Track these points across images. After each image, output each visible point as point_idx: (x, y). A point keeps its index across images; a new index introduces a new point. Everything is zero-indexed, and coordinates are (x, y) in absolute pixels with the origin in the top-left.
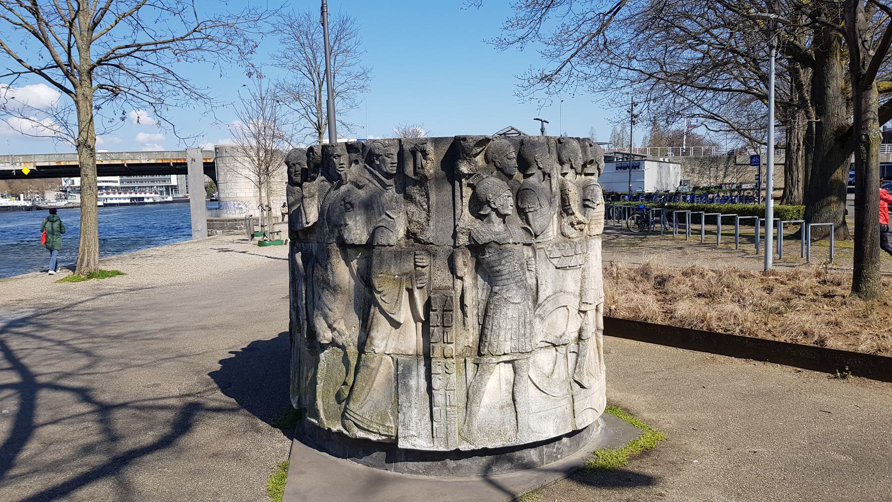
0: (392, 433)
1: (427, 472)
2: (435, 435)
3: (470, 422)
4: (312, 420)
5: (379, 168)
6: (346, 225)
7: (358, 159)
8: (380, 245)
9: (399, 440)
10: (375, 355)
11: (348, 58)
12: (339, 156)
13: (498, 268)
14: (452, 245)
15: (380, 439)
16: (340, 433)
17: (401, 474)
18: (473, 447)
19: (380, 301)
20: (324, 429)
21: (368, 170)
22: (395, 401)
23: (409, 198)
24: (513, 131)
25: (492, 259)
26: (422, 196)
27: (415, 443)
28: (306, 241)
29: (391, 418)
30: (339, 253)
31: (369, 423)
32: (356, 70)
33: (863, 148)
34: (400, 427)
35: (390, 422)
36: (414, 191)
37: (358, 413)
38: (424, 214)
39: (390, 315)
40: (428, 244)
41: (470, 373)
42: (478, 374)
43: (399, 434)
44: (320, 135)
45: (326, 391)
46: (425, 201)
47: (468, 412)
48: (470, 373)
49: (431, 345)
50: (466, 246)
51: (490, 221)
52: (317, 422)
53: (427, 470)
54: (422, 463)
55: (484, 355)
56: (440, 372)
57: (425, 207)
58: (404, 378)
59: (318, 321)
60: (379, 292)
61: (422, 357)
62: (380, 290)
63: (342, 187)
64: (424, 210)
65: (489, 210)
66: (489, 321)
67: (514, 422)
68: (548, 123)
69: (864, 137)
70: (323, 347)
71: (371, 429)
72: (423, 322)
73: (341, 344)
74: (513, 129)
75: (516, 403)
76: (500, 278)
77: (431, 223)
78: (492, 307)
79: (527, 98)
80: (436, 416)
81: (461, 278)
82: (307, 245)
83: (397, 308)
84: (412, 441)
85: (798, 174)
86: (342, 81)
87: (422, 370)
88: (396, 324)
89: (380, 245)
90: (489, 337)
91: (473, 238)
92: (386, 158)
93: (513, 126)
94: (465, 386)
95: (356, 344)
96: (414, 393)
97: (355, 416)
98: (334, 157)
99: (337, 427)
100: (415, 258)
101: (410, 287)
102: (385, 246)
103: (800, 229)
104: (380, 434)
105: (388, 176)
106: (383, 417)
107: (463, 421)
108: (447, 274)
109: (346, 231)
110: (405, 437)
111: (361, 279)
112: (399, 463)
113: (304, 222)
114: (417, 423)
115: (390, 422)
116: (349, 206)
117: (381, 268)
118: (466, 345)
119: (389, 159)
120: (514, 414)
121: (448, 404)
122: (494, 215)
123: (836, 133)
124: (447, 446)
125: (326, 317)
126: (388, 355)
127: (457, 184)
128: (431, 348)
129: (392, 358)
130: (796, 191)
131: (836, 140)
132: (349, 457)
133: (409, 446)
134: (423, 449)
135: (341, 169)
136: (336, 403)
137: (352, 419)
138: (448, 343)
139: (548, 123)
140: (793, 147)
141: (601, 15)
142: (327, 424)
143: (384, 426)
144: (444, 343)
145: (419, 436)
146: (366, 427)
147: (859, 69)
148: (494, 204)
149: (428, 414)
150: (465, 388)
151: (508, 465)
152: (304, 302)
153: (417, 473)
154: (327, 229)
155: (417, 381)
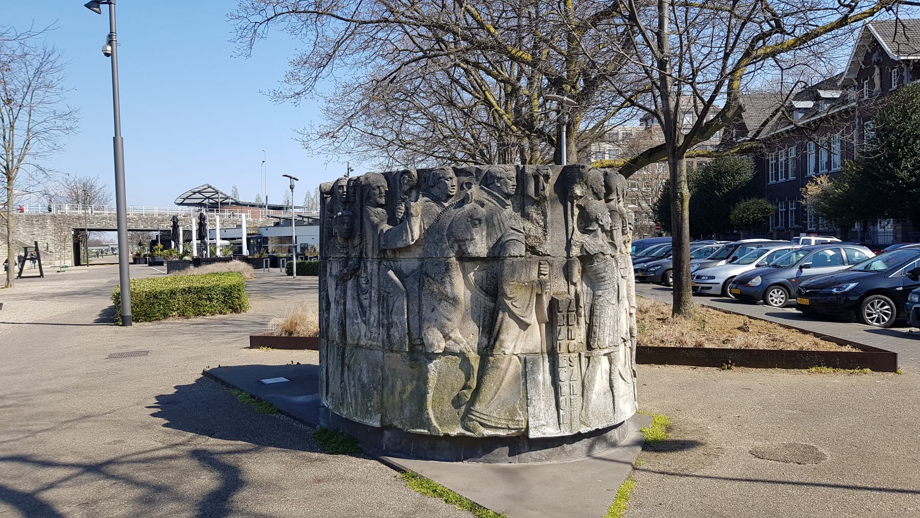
0: (522, 425)
1: (548, 458)
2: (561, 422)
3: (587, 407)
4: (417, 430)
5: (499, 190)
6: (472, 239)
7: (471, 182)
8: (511, 256)
9: (530, 431)
10: (505, 356)
11: (47, 94)
12: (451, 178)
13: (603, 275)
14: (565, 256)
15: (509, 433)
16: (461, 437)
17: (526, 464)
18: (589, 429)
19: (511, 306)
20: (440, 436)
21: (486, 191)
22: (523, 396)
23: (526, 216)
24: (210, 190)
25: (600, 267)
26: (538, 214)
27: (545, 431)
28: (394, 260)
29: (521, 413)
30: (458, 266)
31: (496, 421)
32: (61, 108)
33: (678, 202)
34: (530, 419)
35: (520, 416)
36: (532, 211)
37: (485, 413)
38: (540, 230)
39: (522, 318)
40: (545, 255)
41: (584, 365)
42: (590, 365)
43: (530, 425)
44: (8, 180)
45: (438, 401)
46: (541, 219)
47: (585, 399)
48: (584, 365)
49: (558, 342)
50: (577, 257)
51: (596, 236)
52: (426, 431)
53: (550, 456)
54: (544, 450)
55: (593, 349)
56: (566, 365)
57: (542, 224)
58: (533, 374)
59: (430, 332)
60: (511, 299)
61: (546, 355)
62: (511, 296)
63: (466, 206)
64: (540, 226)
65: (596, 227)
66: (596, 320)
67: (612, 405)
68: (297, 180)
69: (679, 194)
70: (431, 357)
71: (500, 426)
72: (547, 324)
73: (459, 352)
74: (209, 187)
75: (613, 388)
76: (603, 283)
77: (548, 238)
78: (598, 308)
79: (315, 152)
80: (562, 404)
81: (575, 284)
82: (395, 263)
83: (529, 312)
84: (543, 430)
86: (40, 120)
87: (547, 365)
88: (524, 326)
89: (511, 256)
90: (597, 333)
91: (585, 250)
92: (509, 181)
93: (210, 184)
94: (580, 376)
95: (476, 349)
96: (541, 387)
97: (482, 416)
98: (447, 179)
99: (456, 431)
100: (539, 268)
101: (540, 292)
102: (517, 257)
104: (509, 429)
105: (508, 196)
106: (512, 413)
107: (581, 408)
108: (562, 281)
109: (472, 245)
110: (536, 428)
111: (481, 290)
112: (523, 454)
113: (410, 239)
114: (545, 414)
115: (520, 416)
116: (477, 222)
117: (512, 276)
118: (580, 341)
119: (510, 182)
120: (612, 398)
121: (572, 393)
122: (599, 230)
124: (571, 431)
125: (442, 328)
126: (516, 355)
127: (569, 204)
128: (558, 345)
129: (519, 358)
132: (465, 459)
133: (540, 435)
134: (552, 436)
135: (453, 190)
136: (453, 408)
137: (478, 419)
138: (571, 339)
139: (297, 180)
141: (374, 82)
142: (442, 431)
143: (513, 420)
144: (568, 339)
145: (547, 425)
146: (494, 425)
147: (675, 143)
148: (602, 221)
149: (554, 405)
150: (580, 379)
151: (604, 445)
152: (406, 317)
153: (540, 460)
154: (447, 244)
155: (543, 375)
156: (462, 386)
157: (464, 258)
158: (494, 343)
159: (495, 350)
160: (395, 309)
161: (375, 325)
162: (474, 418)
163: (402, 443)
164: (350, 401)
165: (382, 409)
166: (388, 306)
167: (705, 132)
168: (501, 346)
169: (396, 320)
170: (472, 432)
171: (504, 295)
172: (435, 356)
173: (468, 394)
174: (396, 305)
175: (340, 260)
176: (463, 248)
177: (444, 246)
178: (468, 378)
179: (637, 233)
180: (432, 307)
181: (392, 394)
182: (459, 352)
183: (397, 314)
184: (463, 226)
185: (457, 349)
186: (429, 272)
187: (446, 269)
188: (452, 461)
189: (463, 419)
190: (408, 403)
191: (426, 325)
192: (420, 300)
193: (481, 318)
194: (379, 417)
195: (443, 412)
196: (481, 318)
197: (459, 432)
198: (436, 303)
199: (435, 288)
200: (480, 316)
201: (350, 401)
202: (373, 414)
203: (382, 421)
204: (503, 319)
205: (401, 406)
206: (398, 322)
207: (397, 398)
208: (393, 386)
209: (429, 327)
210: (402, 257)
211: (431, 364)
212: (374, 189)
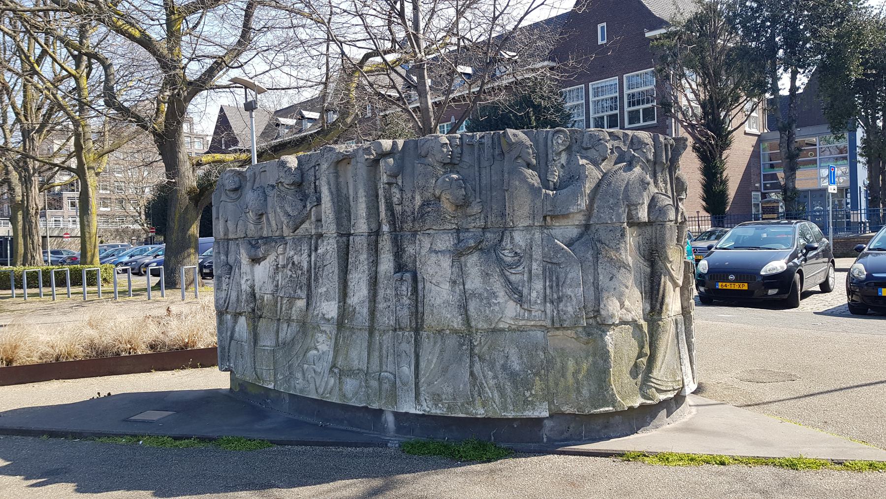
4: (601, 410)
16: (642, 406)
52: (611, 408)
59: (610, 303)
60: (671, 262)
71: (668, 389)
73: (631, 320)
85: (38, 238)
103: (160, 281)
109: (641, 210)
123: (189, 193)
130: (38, 255)
131: (190, 199)
136: (631, 379)
137: (656, 386)
140: (31, 210)
143: (675, 381)
156: (636, 355)
157: (634, 223)
158: (661, 308)
159: (663, 314)
160: (568, 281)
161: (539, 302)
162: (653, 384)
163: (571, 429)
164: (491, 396)
165: (548, 396)
166: (557, 278)
167: (327, 135)
168: (667, 310)
169: (569, 293)
170: (652, 400)
171: (667, 258)
172: (608, 328)
173: (644, 360)
174: (569, 276)
175: (451, 231)
176: (634, 212)
177: (620, 211)
178: (642, 347)
179: (118, 238)
180: (611, 275)
181: (563, 376)
182: (631, 320)
183: (571, 286)
184: (637, 190)
185: (629, 318)
186: (603, 238)
187: (621, 235)
188: (627, 435)
189: (641, 389)
190: (585, 382)
191: (605, 295)
192: (596, 269)
193: (643, 284)
194: (545, 405)
195: (623, 385)
196: (643, 284)
197: (640, 402)
198: (615, 271)
199: (612, 254)
200: (641, 282)
201: (491, 396)
202: (538, 403)
203: (550, 410)
204: (665, 282)
205: (578, 388)
206: (573, 295)
207: (571, 380)
208: (564, 368)
209: (608, 297)
210: (557, 224)
211: (607, 337)
212: (528, 148)
